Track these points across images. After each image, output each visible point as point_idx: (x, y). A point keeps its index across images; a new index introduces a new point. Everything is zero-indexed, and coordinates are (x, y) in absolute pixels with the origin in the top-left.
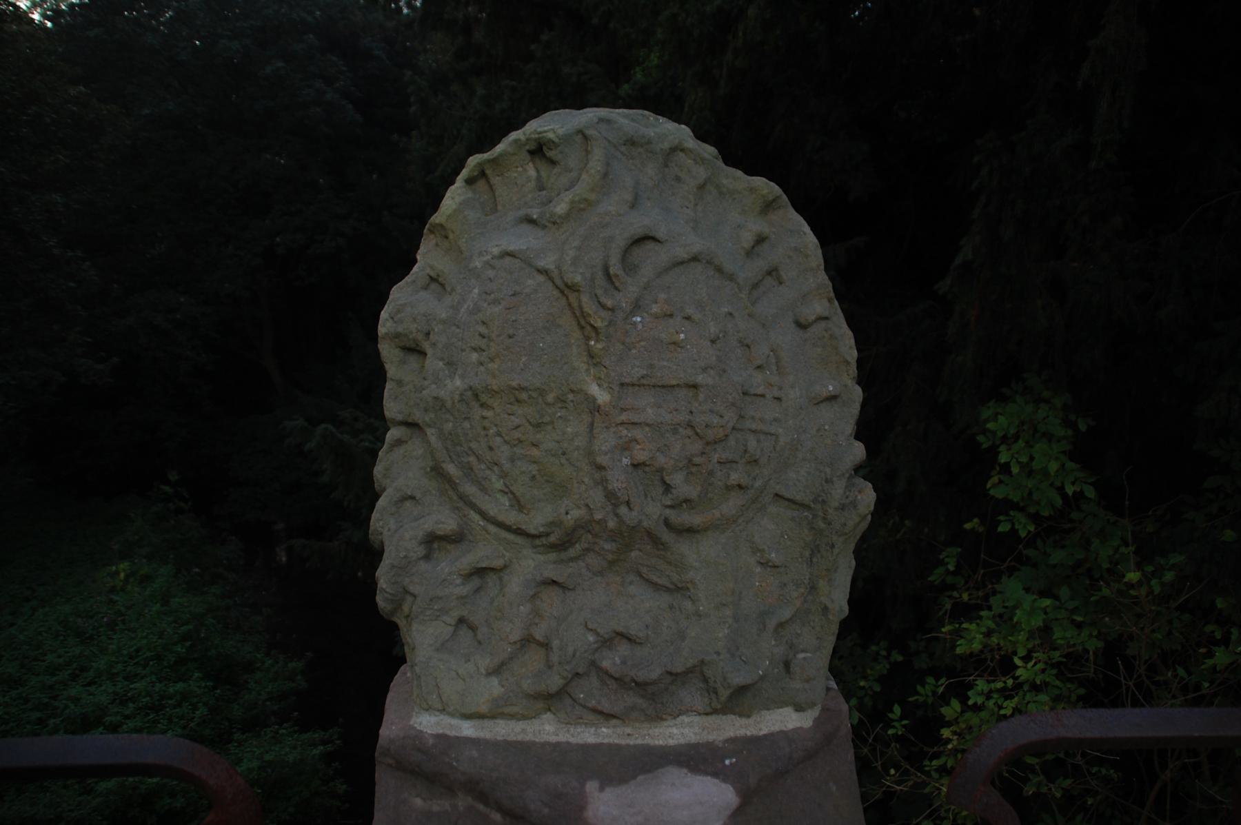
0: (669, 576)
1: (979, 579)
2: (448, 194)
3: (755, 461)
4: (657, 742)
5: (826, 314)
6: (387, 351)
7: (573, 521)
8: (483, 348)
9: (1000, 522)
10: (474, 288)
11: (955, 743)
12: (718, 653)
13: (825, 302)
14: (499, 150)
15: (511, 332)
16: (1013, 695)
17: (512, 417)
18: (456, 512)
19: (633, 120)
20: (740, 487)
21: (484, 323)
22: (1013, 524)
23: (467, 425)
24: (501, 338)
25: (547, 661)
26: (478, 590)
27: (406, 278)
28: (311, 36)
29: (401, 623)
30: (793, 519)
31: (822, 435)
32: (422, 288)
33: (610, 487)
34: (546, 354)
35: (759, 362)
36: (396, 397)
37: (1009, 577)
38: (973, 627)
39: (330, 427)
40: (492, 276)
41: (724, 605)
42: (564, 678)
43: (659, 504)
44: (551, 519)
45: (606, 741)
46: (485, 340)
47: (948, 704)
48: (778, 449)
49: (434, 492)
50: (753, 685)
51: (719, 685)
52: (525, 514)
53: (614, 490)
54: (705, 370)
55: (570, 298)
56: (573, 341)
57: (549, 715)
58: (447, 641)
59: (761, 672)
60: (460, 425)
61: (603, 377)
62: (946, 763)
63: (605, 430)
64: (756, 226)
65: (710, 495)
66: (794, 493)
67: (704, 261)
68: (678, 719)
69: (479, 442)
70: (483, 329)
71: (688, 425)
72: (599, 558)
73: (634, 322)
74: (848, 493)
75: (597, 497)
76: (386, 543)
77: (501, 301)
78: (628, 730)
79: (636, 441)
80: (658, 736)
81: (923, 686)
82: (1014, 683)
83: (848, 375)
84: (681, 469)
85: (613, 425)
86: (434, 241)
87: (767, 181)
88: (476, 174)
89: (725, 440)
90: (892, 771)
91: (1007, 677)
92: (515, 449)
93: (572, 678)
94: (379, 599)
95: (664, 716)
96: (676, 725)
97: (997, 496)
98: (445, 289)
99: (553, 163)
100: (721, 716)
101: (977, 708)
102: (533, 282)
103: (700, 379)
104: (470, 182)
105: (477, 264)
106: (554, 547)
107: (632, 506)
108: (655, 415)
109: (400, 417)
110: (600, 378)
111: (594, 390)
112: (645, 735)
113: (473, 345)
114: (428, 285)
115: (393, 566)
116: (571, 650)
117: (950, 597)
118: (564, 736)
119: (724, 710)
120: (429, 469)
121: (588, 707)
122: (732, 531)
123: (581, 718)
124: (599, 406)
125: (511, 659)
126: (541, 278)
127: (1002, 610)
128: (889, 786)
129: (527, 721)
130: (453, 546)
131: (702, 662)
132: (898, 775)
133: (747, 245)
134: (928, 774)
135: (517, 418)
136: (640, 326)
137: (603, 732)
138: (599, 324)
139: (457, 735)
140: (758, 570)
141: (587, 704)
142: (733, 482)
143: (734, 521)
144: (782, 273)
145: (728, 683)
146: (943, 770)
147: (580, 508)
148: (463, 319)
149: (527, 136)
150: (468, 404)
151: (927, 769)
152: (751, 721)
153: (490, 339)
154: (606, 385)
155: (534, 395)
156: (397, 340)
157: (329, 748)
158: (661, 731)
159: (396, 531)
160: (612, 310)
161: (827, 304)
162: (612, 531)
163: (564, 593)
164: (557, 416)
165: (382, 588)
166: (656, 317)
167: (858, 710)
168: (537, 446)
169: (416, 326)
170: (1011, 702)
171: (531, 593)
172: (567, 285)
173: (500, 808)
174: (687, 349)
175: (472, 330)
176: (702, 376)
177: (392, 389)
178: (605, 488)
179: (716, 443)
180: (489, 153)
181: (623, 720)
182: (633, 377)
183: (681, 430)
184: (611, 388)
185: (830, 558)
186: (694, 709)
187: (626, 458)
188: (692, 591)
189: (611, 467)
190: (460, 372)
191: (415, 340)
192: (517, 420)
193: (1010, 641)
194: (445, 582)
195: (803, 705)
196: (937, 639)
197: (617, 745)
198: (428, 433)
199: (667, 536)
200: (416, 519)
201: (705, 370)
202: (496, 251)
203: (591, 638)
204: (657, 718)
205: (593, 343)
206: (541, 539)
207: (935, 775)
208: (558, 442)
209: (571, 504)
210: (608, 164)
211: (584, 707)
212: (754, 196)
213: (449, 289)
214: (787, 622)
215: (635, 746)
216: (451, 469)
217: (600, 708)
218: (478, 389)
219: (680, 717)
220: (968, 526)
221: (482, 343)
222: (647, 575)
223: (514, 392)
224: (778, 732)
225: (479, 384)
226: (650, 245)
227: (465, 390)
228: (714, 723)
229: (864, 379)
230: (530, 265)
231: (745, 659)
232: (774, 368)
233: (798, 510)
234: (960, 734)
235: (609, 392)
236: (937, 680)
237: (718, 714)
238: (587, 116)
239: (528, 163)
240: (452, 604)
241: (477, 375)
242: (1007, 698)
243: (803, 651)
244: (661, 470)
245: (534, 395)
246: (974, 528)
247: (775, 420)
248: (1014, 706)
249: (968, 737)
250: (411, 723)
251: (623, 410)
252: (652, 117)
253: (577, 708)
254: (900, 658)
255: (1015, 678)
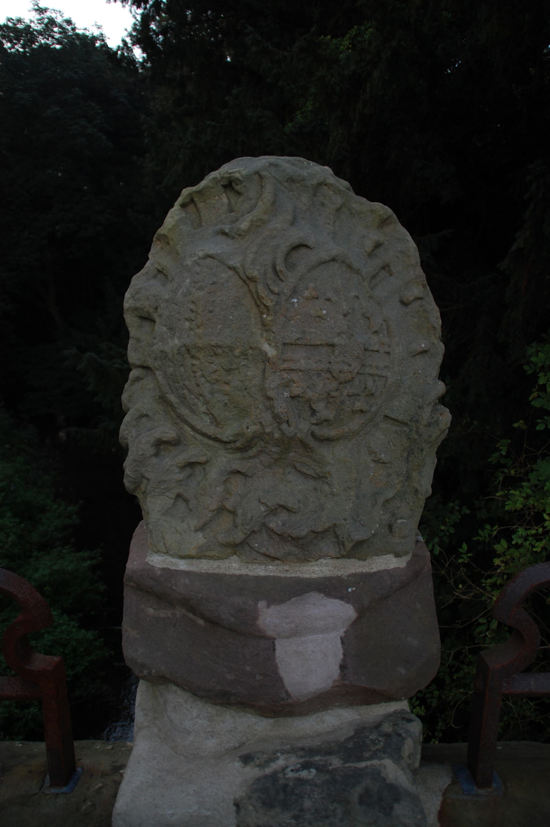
0: (314, 469)
1: (522, 460)
2: (169, 214)
3: (372, 394)
4: (304, 576)
5: (421, 295)
6: (130, 319)
7: (251, 433)
8: (192, 319)
9: (538, 423)
10: (187, 279)
11: (502, 568)
12: (345, 519)
13: (421, 287)
14: (203, 185)
15: (211, 308)
16: (542, 538)
17: (212, 365)
18: (175, 425)
19: (293, 165)
20: (362, 411)
21: (193, 302)
22: (547, 425)
23: (182, 369)
24: (204, 313)
25: (234, 522)
26: (189, 476)
27: (142, 271)
28: (77, 89)
29: (140, 496)
30: (396, 432)
31: (416, 377)
32: (152, 277)
33: (276, 412)
34: (234, 324)
35: (375, 329)
36: (136, 349)
37: (542, 460)
38: (517, 493)
39: (93, 354)
40: (198, 271)
41: (350, 488)
42: (245, 534)
43: (308, 423)
44: (237, 432)
45: (271, 574)
46: (194, 314)
47: (499, 543)
48: (387, 386)
49: (161, 412)
50: (368, 540)
51: (346, 539)
52: (220, 428)
53: (279, 413)
54: (339, 334)
55: (250, 286)
56: (252, 315)
57: (235, 557)
58: (170, 508)
59: (373, 532)
60: (178, 370)
61: (271, 339)
62: (496, 581)
63: (273, 374)
64: (374, 236)
65: (342, 417)
66: (398, 415)
67: (340, 261)
68: (318, 561)
69: (190, 380)
70: (192, 306)
71: (328, 371)
72: (268, 457)
73: (293, 302)
74: (433, 415)
75: (267, 417)
76: (130, 445)
77: (205, 288)
78: (286, 568)
79: (293, 381)
80: (305, 571)
81: (483, 531)
82: (543, 530)
83: (435, 336)
84: (323, 400)
85: (278, 371)
86: (160, 246)
87: (383, 205)
88: (187, 201)
89: (352, 380)
90: (461, 586)
91: (539, 527)
92: (214, 386)
93: (251, 534)
94: (125, 481)
95: (310, 559)
96: (317, 565)
97: (536, 406)
98: (167, 278)
99: (239, 193)
100: (346, 559)
101: (518, 546)
102: (227, 274)
103: (336, 341)
104: (184, 206)
105: (189, 262)
106: (239, 449)
107: (290, 424)
108: (306, 364)
109: (138, 363)
110: (270, 340)
111: (266, 347)
112: (297, 571)
113: (186, 317)
114: (156, 275)
115: (135, 461)
116: (249, 516)
117: (502, 472)
118: (245, 570)
119: (348, 556)
120: (157, 398)
121: (260, 553)
122: (356, 440)
123: (256, 560)
124: (269, 358)
125: (211, 521)
126: (231, 273)
127: (537, 482)
128: (457, 596)
129: (221, 561)
130: (173, 447)
131: (335, 525)
132: (464, 588)
133: (369, 249)
134: (484, 588)
135: (215, 365)
136: (296, 305)
137: (270, 568)
138: (269, 304)
139: (176, 568)
140: (373, 465)
141: (260, 551)
142: (357, 408)
143: (357, 433)
144: (392, 268)
145: (352, 539)
146: (494, 586)
147: (256, 424)
148: (180, 299)
149: (222, 176)
150: (183, 356)
151: (483, 585)
152: (366, 563)
153: (198, 314)
154: (273, 344)
155: (226, 350)
156: (136, 312)
157: (95, 562)
158: (307, 568)
159: (136, 437)
160: (278, 294)
161: (422, 289)
162: (277, 439)
163: (246, 479)
164: (241, 364)
165: (127, 474)
166: (307, 299)
167: (439, 546)
168: (228, 384)
169: (148, 303)
170: (541, 543)
171: (224, 479)
172: (248, 277)
173: (203, 617)
174: (328, 321)
175: (185, 307)
176: (337, 338)
177: (133, 344)
178: (273, 412)
179: (346, 382)
180: (196, 187)
181: (283, 562)
182: (291, 339)
183: (323, 374)
184: (277, 346)
185: (420, 458)
186: (329, 555)
187: (287, 392)
188: (329, 478)
189: (276, 398)
190: (177, 334)
191: (148, 312)
192: (215, 367)
193: (541, 503)
194: (168, 471)
195: (400, 553)
196: (493, 500)
197: (278, 577)
198: (157, 374)
199: (312, 443)
200: (149, 430)
201: (339, 334)
202: (201, 254)
203: (263, 509)
204: (305, 560)
205: (265, 316)
206: (231, 444)
207: (489, 589)
208: (242, 381)
209: (250, 422)
210: (276, 195)
211: (258, 552)
212: (374, 216)
213: (170, 279)
214: (391, 499)
215: (290, 578)
216: (172, 398)
217: (268, 553)
218: (189, 346)
219: (320, 560)
220: (516, 425)
221: (192, 316)
222: (300, 468)
223: (213, 348)
224: (383, 571)
225: (190, 343)
226: (304, 250)
227: (181, 347)
228: (342, 564)
229: (445, 339)
230: (224, 264)
231: (363, 523)
232: (386, 332)
233: (400, 426)
234: (506, 563)
235: (276, 349)
236: (492, 527)
237: (345, 558)
238: (263, 161)
239: (222, 194)
240: (173, 485)
241: (188, 336)
242: (538, 540)
243: (401, 518)
244: (309, 401)
245: (226, 350)
246: (520, 427)
247: (386, 367)
248: (543, 546)
249: (511, 565)
250: (147, 560)
251: (284, 361)
252: (305, 161)
253: (253, 552)
254: (468, 512)
255: (544, 527)
